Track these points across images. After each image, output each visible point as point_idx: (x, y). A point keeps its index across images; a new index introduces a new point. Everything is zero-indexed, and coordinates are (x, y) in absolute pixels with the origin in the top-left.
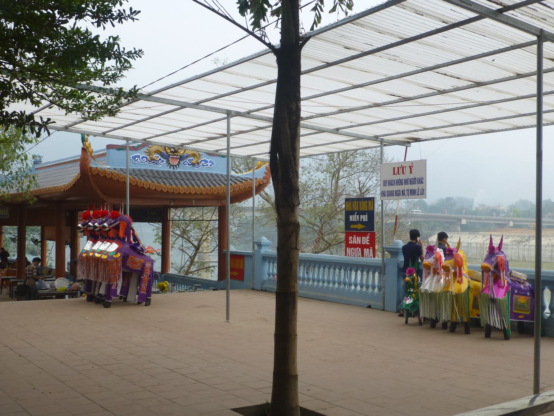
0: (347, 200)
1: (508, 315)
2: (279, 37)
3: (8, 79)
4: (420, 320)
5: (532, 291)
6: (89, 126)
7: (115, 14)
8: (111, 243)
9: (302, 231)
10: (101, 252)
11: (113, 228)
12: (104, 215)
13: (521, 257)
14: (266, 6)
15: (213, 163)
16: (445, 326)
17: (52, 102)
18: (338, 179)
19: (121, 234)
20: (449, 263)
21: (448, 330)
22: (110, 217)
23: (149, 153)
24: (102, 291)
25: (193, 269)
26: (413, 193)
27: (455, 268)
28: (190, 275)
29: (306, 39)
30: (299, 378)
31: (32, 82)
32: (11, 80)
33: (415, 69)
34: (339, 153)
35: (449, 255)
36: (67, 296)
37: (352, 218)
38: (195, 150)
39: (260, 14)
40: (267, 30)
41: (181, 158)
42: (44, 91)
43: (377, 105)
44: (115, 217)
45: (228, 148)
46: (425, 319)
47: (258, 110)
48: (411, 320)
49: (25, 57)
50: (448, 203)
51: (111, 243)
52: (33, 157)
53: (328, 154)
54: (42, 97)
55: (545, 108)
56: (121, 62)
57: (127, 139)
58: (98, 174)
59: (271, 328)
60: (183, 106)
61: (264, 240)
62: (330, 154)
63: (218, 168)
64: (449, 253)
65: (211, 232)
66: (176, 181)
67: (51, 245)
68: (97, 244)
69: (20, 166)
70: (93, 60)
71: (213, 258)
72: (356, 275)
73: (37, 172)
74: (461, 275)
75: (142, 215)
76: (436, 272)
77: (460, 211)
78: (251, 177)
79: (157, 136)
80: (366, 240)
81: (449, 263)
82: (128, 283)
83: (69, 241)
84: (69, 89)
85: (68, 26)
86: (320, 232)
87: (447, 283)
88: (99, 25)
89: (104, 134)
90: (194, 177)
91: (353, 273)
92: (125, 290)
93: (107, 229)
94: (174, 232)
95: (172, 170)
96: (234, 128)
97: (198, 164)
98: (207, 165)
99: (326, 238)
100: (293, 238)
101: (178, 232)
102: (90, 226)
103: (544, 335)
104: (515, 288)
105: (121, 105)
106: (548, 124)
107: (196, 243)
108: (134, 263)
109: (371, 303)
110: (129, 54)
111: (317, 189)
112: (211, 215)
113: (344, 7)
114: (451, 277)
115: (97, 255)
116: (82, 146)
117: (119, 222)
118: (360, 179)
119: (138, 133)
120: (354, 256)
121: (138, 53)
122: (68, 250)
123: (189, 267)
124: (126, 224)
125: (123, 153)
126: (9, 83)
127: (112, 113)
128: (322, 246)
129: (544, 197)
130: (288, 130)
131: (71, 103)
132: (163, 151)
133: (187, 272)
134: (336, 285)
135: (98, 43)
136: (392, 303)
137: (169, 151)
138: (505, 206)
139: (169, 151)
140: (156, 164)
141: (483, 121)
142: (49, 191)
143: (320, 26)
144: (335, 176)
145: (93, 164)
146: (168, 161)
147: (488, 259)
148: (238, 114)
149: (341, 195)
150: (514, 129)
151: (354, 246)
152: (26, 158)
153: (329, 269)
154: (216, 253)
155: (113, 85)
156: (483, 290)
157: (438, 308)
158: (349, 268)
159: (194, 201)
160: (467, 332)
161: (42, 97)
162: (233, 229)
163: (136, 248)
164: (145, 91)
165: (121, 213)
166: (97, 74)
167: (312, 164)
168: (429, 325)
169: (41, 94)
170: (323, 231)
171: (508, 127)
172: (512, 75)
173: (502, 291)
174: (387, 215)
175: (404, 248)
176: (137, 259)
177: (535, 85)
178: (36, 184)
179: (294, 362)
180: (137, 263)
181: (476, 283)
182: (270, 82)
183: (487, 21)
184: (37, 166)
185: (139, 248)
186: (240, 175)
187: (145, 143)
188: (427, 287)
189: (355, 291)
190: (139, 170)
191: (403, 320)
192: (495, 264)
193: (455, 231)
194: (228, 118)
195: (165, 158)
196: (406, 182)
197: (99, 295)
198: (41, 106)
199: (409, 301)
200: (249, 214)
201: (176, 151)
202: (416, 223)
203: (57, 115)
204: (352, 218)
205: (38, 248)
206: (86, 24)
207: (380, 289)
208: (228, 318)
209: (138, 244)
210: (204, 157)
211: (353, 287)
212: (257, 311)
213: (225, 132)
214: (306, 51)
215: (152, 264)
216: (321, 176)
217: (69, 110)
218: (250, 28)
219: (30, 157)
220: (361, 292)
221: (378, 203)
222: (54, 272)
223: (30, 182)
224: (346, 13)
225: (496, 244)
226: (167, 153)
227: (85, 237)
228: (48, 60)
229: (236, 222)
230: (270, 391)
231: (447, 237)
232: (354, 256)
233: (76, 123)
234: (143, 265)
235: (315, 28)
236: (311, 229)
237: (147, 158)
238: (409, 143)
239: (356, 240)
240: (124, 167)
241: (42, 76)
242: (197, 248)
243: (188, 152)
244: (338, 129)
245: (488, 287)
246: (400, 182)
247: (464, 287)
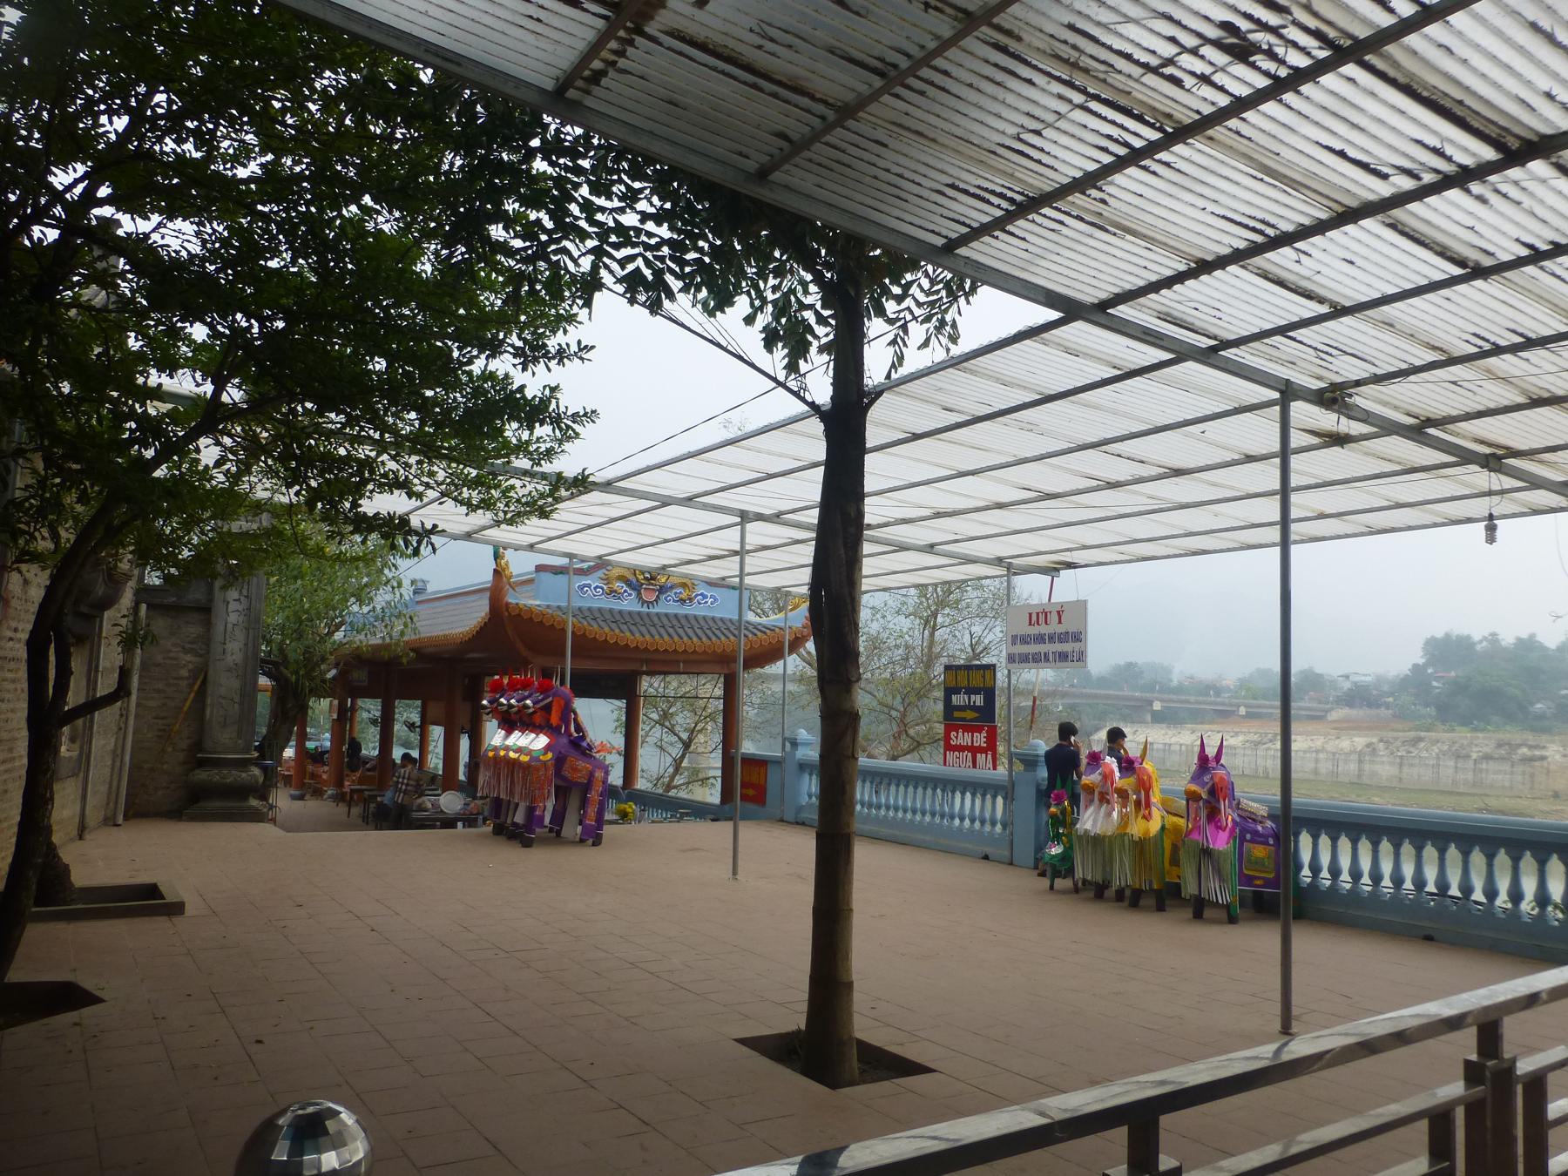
0: (948, 668)
1: (1236, 879)
2: (829, 391)
3: (373, 454)
4: (1076, 884)
5: (1276, 837)
6: (504, 534)
7: (553, 351)
9: (863, 722)
10: (519, 750)
12: (526, 685)
13: (1261, 770)
14: (810, 338)
16: (1120, 896)
17: (443, 494)
18: (934, 629)
20: (1127, 783)
21: (1126, 903)
22: (538, 690)
23: (608, 580)
24: (519, 818)
25: (678, 780)
26: (1063, 657)
27: (1137, 793)
28: (672, 793)
29: (878, 393)
30: (855, 985)
31: (413, 459)
32: (378, 455)
33: (1066, 446)
34: (936, 585)
35: (1127, 769)
36: (460, 824)
37: (958, 700)
38: (686, 576)
39: (798, 351)
40: (809, 379)
41: (662, 590)
42: (431, 474)
43: (1000, 506)
44: (545, 689)
45: (742, 575)
46: (1084, 881)
47: (794, 511)
48: (1060, 883)
49: (402, 419)
50: (1128, 672)
52: (413, 582)
53: (916, 586)
54: (427, 485)
55: (1295, 513)
56: (561, 429)
57: (571, 556)
59: (805, 892)
60: (666, 502)
61: (803, 734)
62: (921, 588)
63: (722, 607)
64: (1127, 765)
65: (712, 717)
66: (653, 630)
67: (437, 733)
69: (388, 597)
70: (515, 425)
71: (715, 762)
72: (963, 799)
73: (419, 607)
74: (1148, 805)
75: (591, 686)
76: (1104, 799)
77: (1150, 687)
78: (782, 625)
79: (621, 551)
80: (980, 739)
81: (1127, 783)
82: (561, 806)
83: (468, 727)
84: (474, 473)
85: (477, 367)
86: (903, 723)
87: (1124, 819)
88: (524, 369)
89: (531, 547)
90: (684, 622)
91: (958, 795)
92: (559, 818)
94: (648, 716)
95: (645, 609)
96: (752, 540)
97: (691, 599)
99: (911, 732)
100: (848, 738)
101: (655, 716)
103: (1300, 915)
104: (1246, 829)
105: (558, 500)
106: (1303, 541)
107: (685, 736)
108: (575, 770)
109: (988, 850)
110: (575, 417)
111: (897, 647)
112: (711, 688)
113: (944, 341)
114: (1130, 808)
115: (512, 755)
118: (974, 629)
119: (589, 546)
120: (959, 767)
121: (590, 416)
122: (464, 743)
123: (672, 778)
125: (562, 579)
126: (375, 460)
127: (544, 514)
128: (905, 744)
129: (1295, 667)
130: (842, 551)
131: (476, 496)
132: (631, 577)
133: (669, 787)
134: (928, 818)
135: (524, 397)
136: (1025, 852)
138: (1231, 678)
141: (1186, 535)
142: (433, 642)
143: (903, 371)
144: (930, 623)
145: (511, 598)
146: (639, 594)
147: (1196, 778)
148: (760, 517)
149: (939, 656)
150: (1242, 549)
151: (961, 748)
152: (400, 585)
153: (916, 788)
154: (719, 754)
155: (546, 467)
156: (1189, 833)
157: (1107, 863)
158: (949, 787)
160: (1160, 908)
161: (427, 485)
162: (748, 712)
163: (579, 745)
164: (599, 478)
165: (556, 682)
166: (522, 448)
167: (890, 602)
168: (1092, 894)
169: (426, 479)
170: (908, 720)
171: (1231, 546)
172: (1236, 457)
173: (1223, 836)
174: (1020, 693)
175: (1048, 754)
176: (581, 764)
177: (1277, 473)
178: (414, 629)
179: (847, 957)
181: (1175, 819)
182: (815, 465)
183: (1190, 364)
184: (420, 598)
185: (584, 744)
186: (764, 620)
187: (601, 563)
188: (1088, 826)
189: (960, 829)
190: (589, 609)
191: (1046, 882)
192: (1210, 787)
193: (1142, 722)
194: (742, 524)
196: (1051, 638)
197: (514, 824)
198: (426, 500)
199: (1056, 850)
200: (777, 687)
201: (653, 578)
202: (1073, 707)
203: (449, 515)
204: (958, 700)
205: (415, 737)
206: (504, 365)
207: (1004, 826)
208: (735, 872)
209: (583, 738)
211: (957, 822)
212: (784, 857)
213: (737, 547)
214: (876, 414)
215: (607, 773)
216: (904, 623)
217: (471, 507)
218: (781, 376)
219: (406, 583)
220: (971, 830)
221: (1001, 676)
222: (439, 781)
223: (406, 625)
224: (948, 350)
225: (1211, 752)
227: (495, 722)
228: (438, 425)
229: (756, 700)
230: (804, 1007)
231: (1123, 735)
232: (959, 767)
233: (485, 528)
235: (894, 376)
236: (883, 717)
238: (1058, 570)
239: (962, 738)
240: (564, 604)
241: (426, 447)
242: (687, 745)
243: (674, 580)
244: (932, 546)
245: (1197, 828)
246: (1040, 639)
247: (1154, 826)
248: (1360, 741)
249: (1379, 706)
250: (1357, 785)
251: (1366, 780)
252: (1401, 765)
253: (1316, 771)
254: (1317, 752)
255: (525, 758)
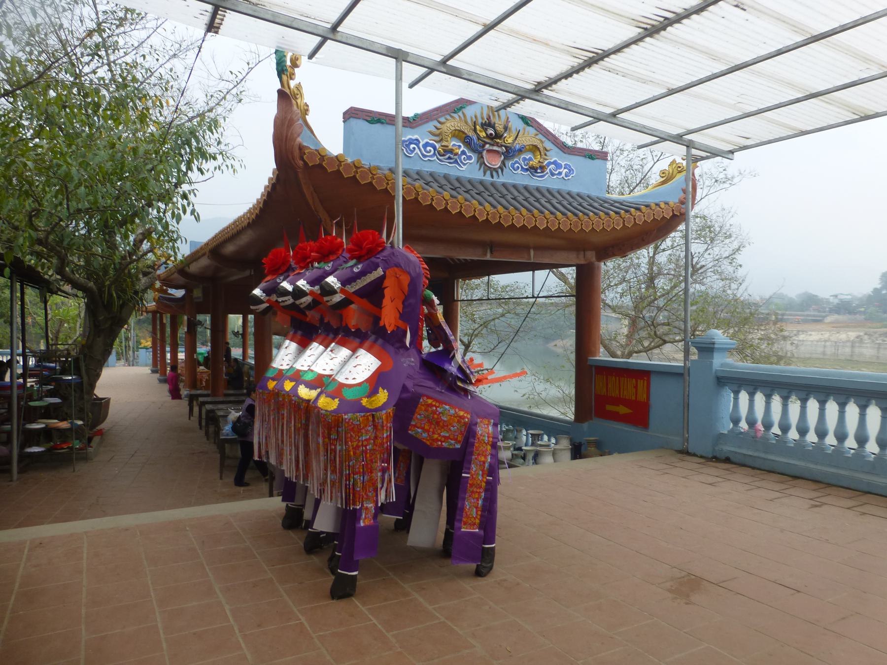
8: (354, 351)
10: (319, 382)
11: (361, 293)
12: (328, 252)
15: (571, 170)
19: (389, 317)
23: (440, 136)
41: (509, 153)
51: (354, 351)
58: (320, 166)
68: (308, 352)
93: (338, 298)
95: (488, 177)
97: (542, 168)
98: (560, 173)
102: (285, 293)
108: (437, 422)
115: (304, 392)
116: (279, 86)
117: (380, 272)
124: (405, 280)
132: (471, 134)
137: (483, 134)
139: (483, 134)
140: (456, 162)
159: (532, 252)
176: (450, 410)
180: (446, 426)
185: (452, 369)
195: (474, 151)
210: (555, 155)
226: (479, 138)
234: (470, 433)
237: (435, 148)
248: (852, 335)
249: (855, 314)
250: (851, 361)
251: (855, 358)
252: (879, 348)
253: (824, 353)
254: (825, 341)
255: (327, 404)
